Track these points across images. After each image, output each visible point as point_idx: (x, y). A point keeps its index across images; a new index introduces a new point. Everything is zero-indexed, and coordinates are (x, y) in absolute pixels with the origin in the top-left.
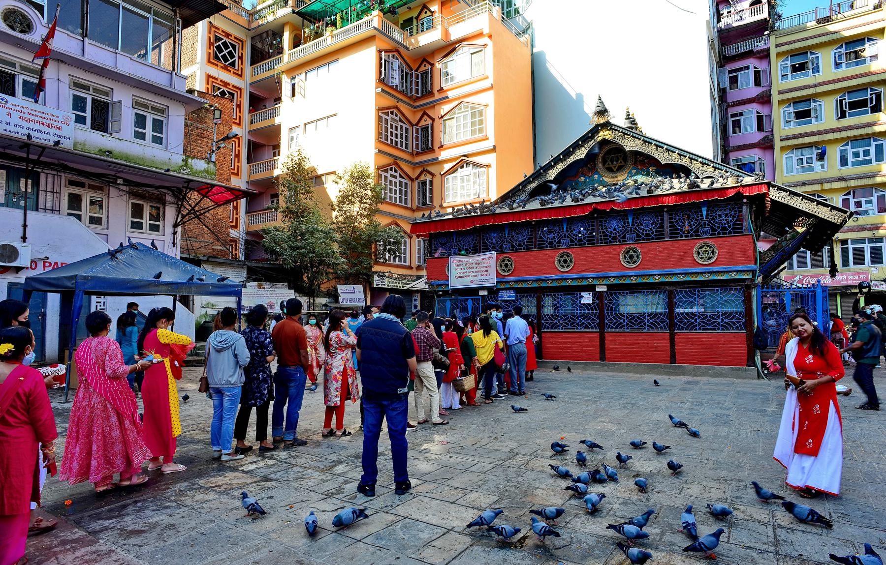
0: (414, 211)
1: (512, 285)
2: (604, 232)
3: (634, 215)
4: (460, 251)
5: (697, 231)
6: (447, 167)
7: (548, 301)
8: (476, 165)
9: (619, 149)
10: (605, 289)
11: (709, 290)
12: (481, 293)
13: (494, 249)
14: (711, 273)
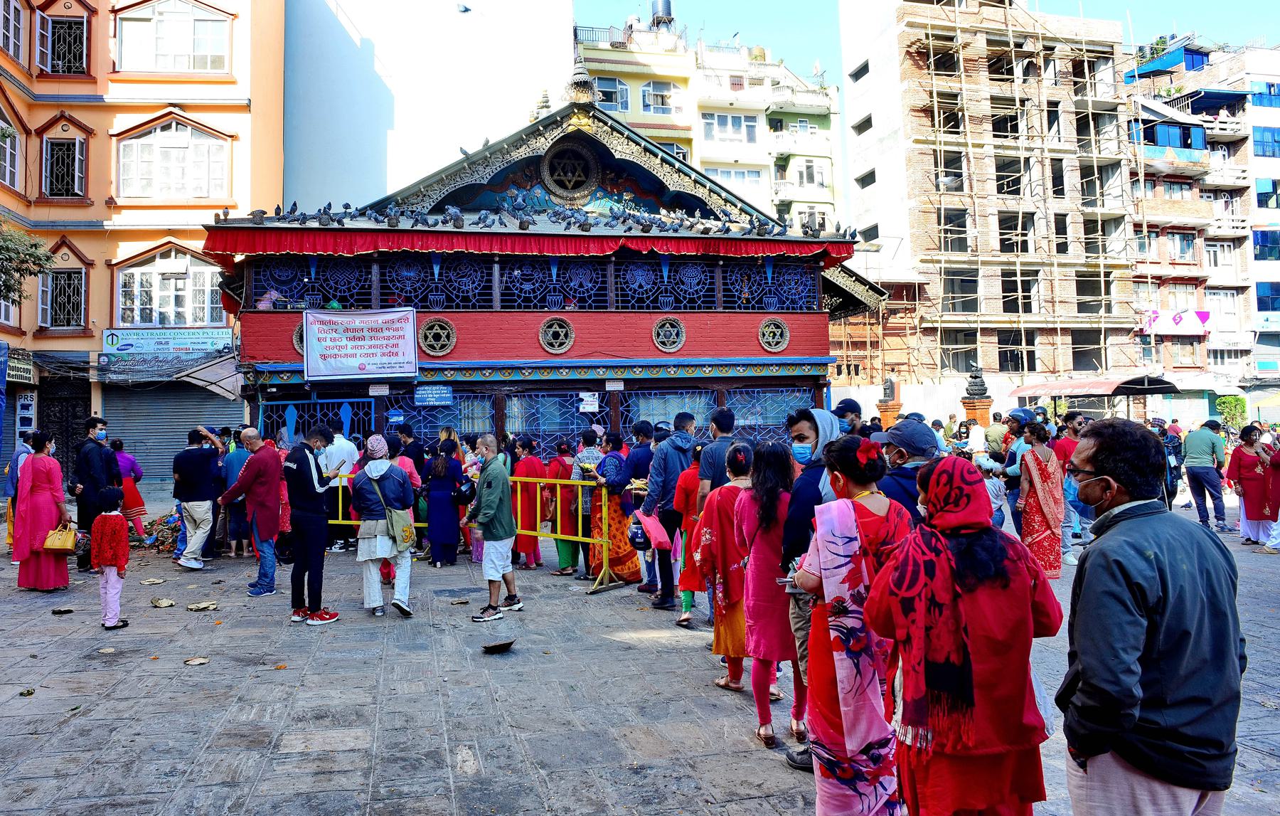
0: (29, 204)
1: (450, 376)
2: (622, 289)
3: (671, 265)
4: (327, 300)
5: (760, 301)
6: (122, 122)
7: (515, 408)
8: (201, 129)
9: (603, 153)
10: (620, 386)
11: (770, 392)
12: (374, 391)
13: (408, 302)
14: (493, 369)
